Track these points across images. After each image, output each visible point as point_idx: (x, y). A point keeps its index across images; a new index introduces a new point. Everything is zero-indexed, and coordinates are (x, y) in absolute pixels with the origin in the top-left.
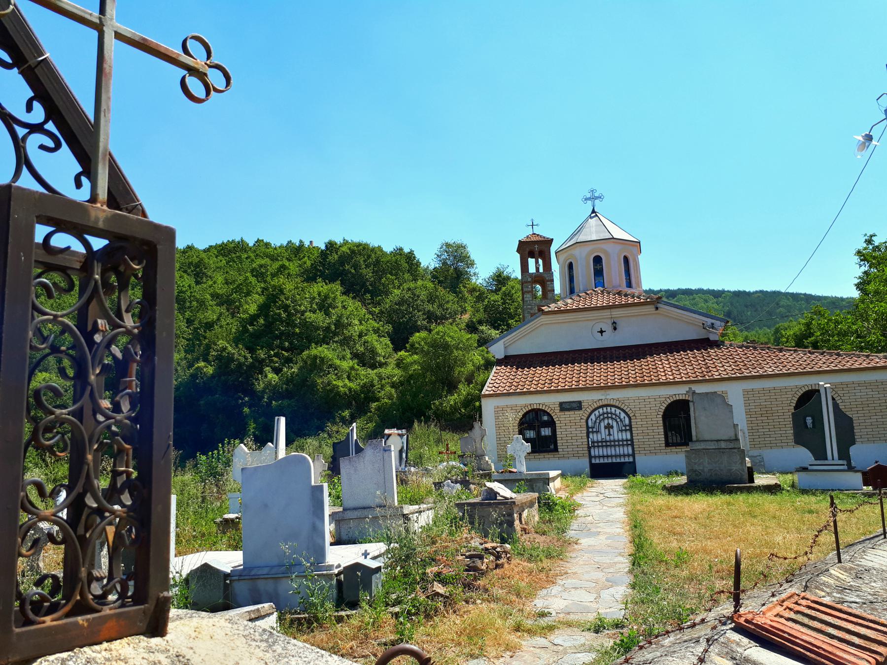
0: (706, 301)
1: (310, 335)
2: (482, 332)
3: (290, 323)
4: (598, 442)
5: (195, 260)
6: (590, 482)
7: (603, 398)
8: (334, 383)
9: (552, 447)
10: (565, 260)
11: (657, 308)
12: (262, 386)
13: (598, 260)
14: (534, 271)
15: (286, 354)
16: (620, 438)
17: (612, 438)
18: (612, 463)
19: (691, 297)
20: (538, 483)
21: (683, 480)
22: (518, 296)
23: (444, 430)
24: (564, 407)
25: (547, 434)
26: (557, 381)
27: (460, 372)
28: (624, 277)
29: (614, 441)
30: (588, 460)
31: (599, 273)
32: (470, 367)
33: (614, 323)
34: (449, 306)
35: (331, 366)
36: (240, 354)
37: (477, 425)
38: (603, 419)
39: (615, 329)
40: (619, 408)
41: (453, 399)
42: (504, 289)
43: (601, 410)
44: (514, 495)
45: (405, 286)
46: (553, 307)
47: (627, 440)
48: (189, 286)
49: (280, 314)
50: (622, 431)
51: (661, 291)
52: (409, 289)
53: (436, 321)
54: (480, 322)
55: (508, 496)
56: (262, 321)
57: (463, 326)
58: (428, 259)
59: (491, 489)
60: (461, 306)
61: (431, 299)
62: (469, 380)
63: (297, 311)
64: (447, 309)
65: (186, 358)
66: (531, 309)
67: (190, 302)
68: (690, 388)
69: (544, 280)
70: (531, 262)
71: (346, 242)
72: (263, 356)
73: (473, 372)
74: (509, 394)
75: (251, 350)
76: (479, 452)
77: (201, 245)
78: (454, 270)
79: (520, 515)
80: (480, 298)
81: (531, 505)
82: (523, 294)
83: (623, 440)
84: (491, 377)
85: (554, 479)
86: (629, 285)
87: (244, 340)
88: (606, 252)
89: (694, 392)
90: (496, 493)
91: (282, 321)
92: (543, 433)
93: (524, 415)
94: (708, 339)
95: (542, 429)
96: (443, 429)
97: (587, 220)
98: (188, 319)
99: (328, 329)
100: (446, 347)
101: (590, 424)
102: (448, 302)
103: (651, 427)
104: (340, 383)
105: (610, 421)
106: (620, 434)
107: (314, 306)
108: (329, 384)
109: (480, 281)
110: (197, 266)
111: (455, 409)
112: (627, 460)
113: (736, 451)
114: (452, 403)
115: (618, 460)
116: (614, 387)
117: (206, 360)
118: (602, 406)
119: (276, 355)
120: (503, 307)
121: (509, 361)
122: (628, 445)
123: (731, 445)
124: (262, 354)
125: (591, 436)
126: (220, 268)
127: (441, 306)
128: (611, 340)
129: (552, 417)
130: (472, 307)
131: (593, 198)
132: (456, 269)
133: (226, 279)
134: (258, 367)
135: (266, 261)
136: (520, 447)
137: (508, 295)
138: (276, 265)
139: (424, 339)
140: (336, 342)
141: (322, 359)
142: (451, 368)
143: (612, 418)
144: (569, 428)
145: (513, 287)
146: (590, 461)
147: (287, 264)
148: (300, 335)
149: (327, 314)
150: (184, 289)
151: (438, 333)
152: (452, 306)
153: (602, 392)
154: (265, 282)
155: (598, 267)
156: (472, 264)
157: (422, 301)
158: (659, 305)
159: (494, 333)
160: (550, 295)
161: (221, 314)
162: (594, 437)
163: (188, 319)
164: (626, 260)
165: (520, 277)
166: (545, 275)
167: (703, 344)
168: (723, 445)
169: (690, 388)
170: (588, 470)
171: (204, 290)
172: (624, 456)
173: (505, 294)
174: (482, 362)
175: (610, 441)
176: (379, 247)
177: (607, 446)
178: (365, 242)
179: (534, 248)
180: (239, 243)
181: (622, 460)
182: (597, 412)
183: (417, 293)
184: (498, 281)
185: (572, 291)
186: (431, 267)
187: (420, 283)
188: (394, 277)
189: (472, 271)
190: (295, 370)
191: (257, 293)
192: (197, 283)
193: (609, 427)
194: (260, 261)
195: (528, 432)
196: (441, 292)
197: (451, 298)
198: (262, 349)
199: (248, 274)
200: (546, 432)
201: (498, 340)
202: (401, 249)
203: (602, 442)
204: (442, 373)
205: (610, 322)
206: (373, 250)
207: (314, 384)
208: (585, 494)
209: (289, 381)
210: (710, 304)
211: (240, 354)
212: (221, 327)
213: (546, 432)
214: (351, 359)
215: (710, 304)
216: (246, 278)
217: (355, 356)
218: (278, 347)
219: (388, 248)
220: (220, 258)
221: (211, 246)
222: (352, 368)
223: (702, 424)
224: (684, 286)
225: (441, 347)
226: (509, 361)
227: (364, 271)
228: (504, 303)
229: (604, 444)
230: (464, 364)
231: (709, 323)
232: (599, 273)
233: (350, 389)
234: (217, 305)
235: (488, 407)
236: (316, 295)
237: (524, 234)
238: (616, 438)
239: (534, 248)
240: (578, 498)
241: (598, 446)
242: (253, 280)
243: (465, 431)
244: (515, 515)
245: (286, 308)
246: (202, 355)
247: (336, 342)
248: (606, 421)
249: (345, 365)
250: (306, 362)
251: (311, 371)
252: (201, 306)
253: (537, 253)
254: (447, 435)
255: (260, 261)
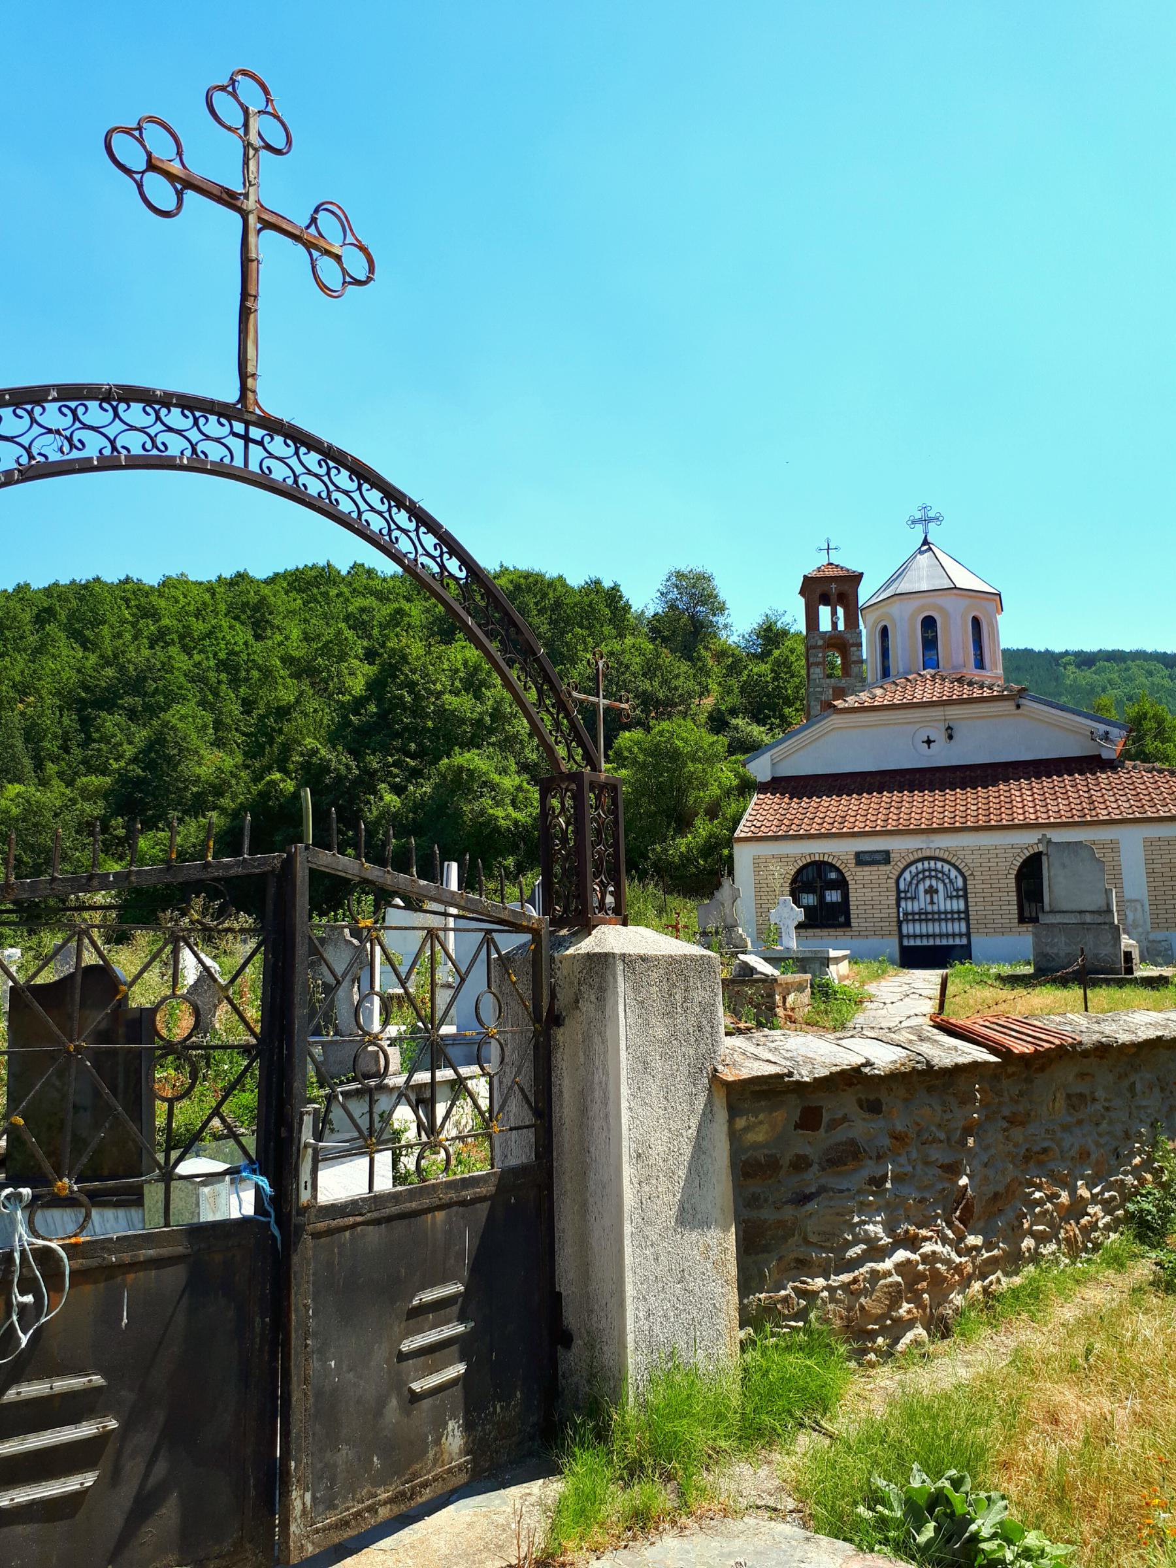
0: (1150, 673)
1: (450, 734)
2: (736, 728)
3: (417, 711)
4: (913, 914)
5: (253, 599)
6: (891, 970)
7: (923, 846)
8: (491, 811)
9: (842, 919)
10: (876, 623)
11: (1018, 707)
12: (375, 813)
13: (929, 623)
14: (829, 629)
15: (412, 763)
16: (949, 908)
17: (935, 908)
18: (935, 947)
19: (1123, 666)
20: (817, 963)
21: (1029, 970)
22: (800, 666)
23: (670, 893)
24: (861, 859)
25: (834, 899)
26: (852, 820)
27: (697, 798)
28: (972, 657)
29: (939, 913)
30: (897, 941)
31: (930, 643)
32: (715, 790)
33: (949, 728)
34: (679, 682)
35: (485, 784)
36: (338, 760)
37: (726, 882)
38: (924, 879)
39: (951, 737)
40: (949, 863)
41: (684, 843)
42: (776, 653)
43: (920, 865)
44: (776, 973)
45: (604, 648)
46: (851, 701)
47: (959, 912)
48: (246, 643)
49: (402, 697)
50: (951, 897)
51: (1067, 653)
52: (611, 654)
53: (656, 708)
54: (733, 712)
55: (769, 973)
56: (373, 708)
57: (703, 718)
58: (644, 598)
59: (746, 963)
60: (699, 684)
61: (649, 671)
62: (712, 812)
63: (430, 692)
64: (676, 688)
65: (247, 767)
66: (821, 693)
67: (248, 671)
68: (1044, 835)
69: (843, 644)
70: (824, 612)
71: (504, 571)
72: (375, 765)
73: (719, 799)
74: (776, 838)
75: (356, 754)
76: (730, 921)
77: (260, 572)
78: (688, 621)
79: (784, 999)
80: (734, 668)
81: (800, 988)
82: (809, 666)
83: (952, 912)
84: (749, 810)
85: (837, 960)
86: (980, 665)
87: (345, 737)
88: (941, 609)
89: (1049, 841)
90: (752, 970)
91: (405, 709)
92: (828, 899)
93: (800, 871)
94: (1100, 755)
95: (827, 893)
96: (668, 891)
97: (913, 557)
98: (243, 700)
99: (479, 723)
100: (675, 755)
101: (902, 887)
102: (678, 676)
103: (997, 895)
104: (499, 812)
105: (934, 882)
106: (948, 902)
107: (457, 684)
108: (482, 812)
109: (733, 639)
110: (256, 608)
111: (687, 859)
112: (957, 942)
113: (1107, 927)
114: (683, 849)
115: (944, 942)
116: (942, 830)
117: (283, 770)
118: (922, 860)
119: (395, 764)
120: (776, 686)
121: (780, 785)
122: (960, 919)
123: (1100, 919)
124: (374, 763)
125: (903, 904)
126: (293, 612)
127: (665, 682)
128: (943, 755)
129: (843, 874)
130: (719, 684)
131: (926, 521)
132: (692, 617)
133: (305, 633)
134: (368, 782)
135: (370, 601)
136: (790, 914)
137: (783, 664)
138: (387, 609)
139: (638, 743)
140: (493, 744)
141: (471, 773)
142: (682, 792)
143: (937, 878)
144: (869, 892)
145: (792, 651)
146: (901, 942)
147: (406, 606)
148: (435, 732)
149: (478, 697)
150: (237, 649)
151: (661, 733)
152: (684, 684)
153: (924, 837)
154: (370, 637)
155: (930, 635)
156: (721, 609)
157: (633, 674)
158: (1022, 701)
159: (757, 731)
160: (855, 669)
161: (302, 693)
162: (908, 906)
163: (243, 700)
164: (976, 622)
165: (804, 633)
166: (848, 636)
167: (1091, 764)
168: (1088, 918)
169: (1044, 835)
170: (897, 955)
171: (269, 650)
172: (954, 935)
173: (777, 662)
174: (735, 783)
175: (933, 913)
176: (560, 577)
177: (927, 920)
178: (537, 569)
179: (830, 588)
180: (323, 569)
181: (951, 942)
182: (913, 869)
183: (626, 661)
184: (766, 638)
185: (886, 673)
186: (650, 613)
187: (629, 640)
188: (585, 632)
189: (721, 620)
190: (427, 789)
191: (356, 657)
192: (258, 637)
193: (931, 891)
194: (360, 602)
195: (805, 895)
196: (667, 657)
197: (684, 668)
198: (373, 754)
199: (342, 625)
200: (833, 896)
201: (769, 747)
202: (598, 582)
203: (920, 914)
204: (668, 798)
205: (942, 726)
206: (551, 584)
207: (459, 813)
208: (883, 983)
209: (418, 806)
210: (1157, 679)
211: (338, 760)
212: (306, 715)
213: (833, 896)
214: (518, 773)
215: (1157, 679)
216: (339, 632)
217: (524, 767)
218: (398, 750)
219: (576, 580)
220: (293, 594)
221: (277, 575)
222: (519, 788)
223: (1058, 885)
224: (1110, 646)
225: (667, 757)
226: (780, 785)
227: (536, 621)
228: (775, 679)
229: (923, 917)
230: (704, 785)
231: (1101, 732)
232: (930, 643)
233: (516, 823)
234: (291, 676)
235: (743, 856)
236: (460, 665)
237: (812, 563)
238: (942, 908)
239: (830, 588)
240: (871, 988)
241: (914, 921)
242: (350, 634)
243: (703, 896)
244: (777, 997)
245: (411, 686)
246: (277, 762)
247: (493, 744)
248: (927, 883)
249: (508, 782)
250: (444, 777)
251: (453, 792)
252: (266, 677)
253: (834, 598)
254: (674, 902)
255: (360, 602)
